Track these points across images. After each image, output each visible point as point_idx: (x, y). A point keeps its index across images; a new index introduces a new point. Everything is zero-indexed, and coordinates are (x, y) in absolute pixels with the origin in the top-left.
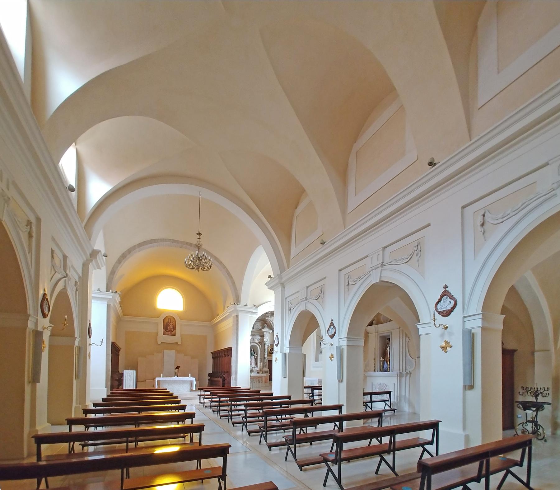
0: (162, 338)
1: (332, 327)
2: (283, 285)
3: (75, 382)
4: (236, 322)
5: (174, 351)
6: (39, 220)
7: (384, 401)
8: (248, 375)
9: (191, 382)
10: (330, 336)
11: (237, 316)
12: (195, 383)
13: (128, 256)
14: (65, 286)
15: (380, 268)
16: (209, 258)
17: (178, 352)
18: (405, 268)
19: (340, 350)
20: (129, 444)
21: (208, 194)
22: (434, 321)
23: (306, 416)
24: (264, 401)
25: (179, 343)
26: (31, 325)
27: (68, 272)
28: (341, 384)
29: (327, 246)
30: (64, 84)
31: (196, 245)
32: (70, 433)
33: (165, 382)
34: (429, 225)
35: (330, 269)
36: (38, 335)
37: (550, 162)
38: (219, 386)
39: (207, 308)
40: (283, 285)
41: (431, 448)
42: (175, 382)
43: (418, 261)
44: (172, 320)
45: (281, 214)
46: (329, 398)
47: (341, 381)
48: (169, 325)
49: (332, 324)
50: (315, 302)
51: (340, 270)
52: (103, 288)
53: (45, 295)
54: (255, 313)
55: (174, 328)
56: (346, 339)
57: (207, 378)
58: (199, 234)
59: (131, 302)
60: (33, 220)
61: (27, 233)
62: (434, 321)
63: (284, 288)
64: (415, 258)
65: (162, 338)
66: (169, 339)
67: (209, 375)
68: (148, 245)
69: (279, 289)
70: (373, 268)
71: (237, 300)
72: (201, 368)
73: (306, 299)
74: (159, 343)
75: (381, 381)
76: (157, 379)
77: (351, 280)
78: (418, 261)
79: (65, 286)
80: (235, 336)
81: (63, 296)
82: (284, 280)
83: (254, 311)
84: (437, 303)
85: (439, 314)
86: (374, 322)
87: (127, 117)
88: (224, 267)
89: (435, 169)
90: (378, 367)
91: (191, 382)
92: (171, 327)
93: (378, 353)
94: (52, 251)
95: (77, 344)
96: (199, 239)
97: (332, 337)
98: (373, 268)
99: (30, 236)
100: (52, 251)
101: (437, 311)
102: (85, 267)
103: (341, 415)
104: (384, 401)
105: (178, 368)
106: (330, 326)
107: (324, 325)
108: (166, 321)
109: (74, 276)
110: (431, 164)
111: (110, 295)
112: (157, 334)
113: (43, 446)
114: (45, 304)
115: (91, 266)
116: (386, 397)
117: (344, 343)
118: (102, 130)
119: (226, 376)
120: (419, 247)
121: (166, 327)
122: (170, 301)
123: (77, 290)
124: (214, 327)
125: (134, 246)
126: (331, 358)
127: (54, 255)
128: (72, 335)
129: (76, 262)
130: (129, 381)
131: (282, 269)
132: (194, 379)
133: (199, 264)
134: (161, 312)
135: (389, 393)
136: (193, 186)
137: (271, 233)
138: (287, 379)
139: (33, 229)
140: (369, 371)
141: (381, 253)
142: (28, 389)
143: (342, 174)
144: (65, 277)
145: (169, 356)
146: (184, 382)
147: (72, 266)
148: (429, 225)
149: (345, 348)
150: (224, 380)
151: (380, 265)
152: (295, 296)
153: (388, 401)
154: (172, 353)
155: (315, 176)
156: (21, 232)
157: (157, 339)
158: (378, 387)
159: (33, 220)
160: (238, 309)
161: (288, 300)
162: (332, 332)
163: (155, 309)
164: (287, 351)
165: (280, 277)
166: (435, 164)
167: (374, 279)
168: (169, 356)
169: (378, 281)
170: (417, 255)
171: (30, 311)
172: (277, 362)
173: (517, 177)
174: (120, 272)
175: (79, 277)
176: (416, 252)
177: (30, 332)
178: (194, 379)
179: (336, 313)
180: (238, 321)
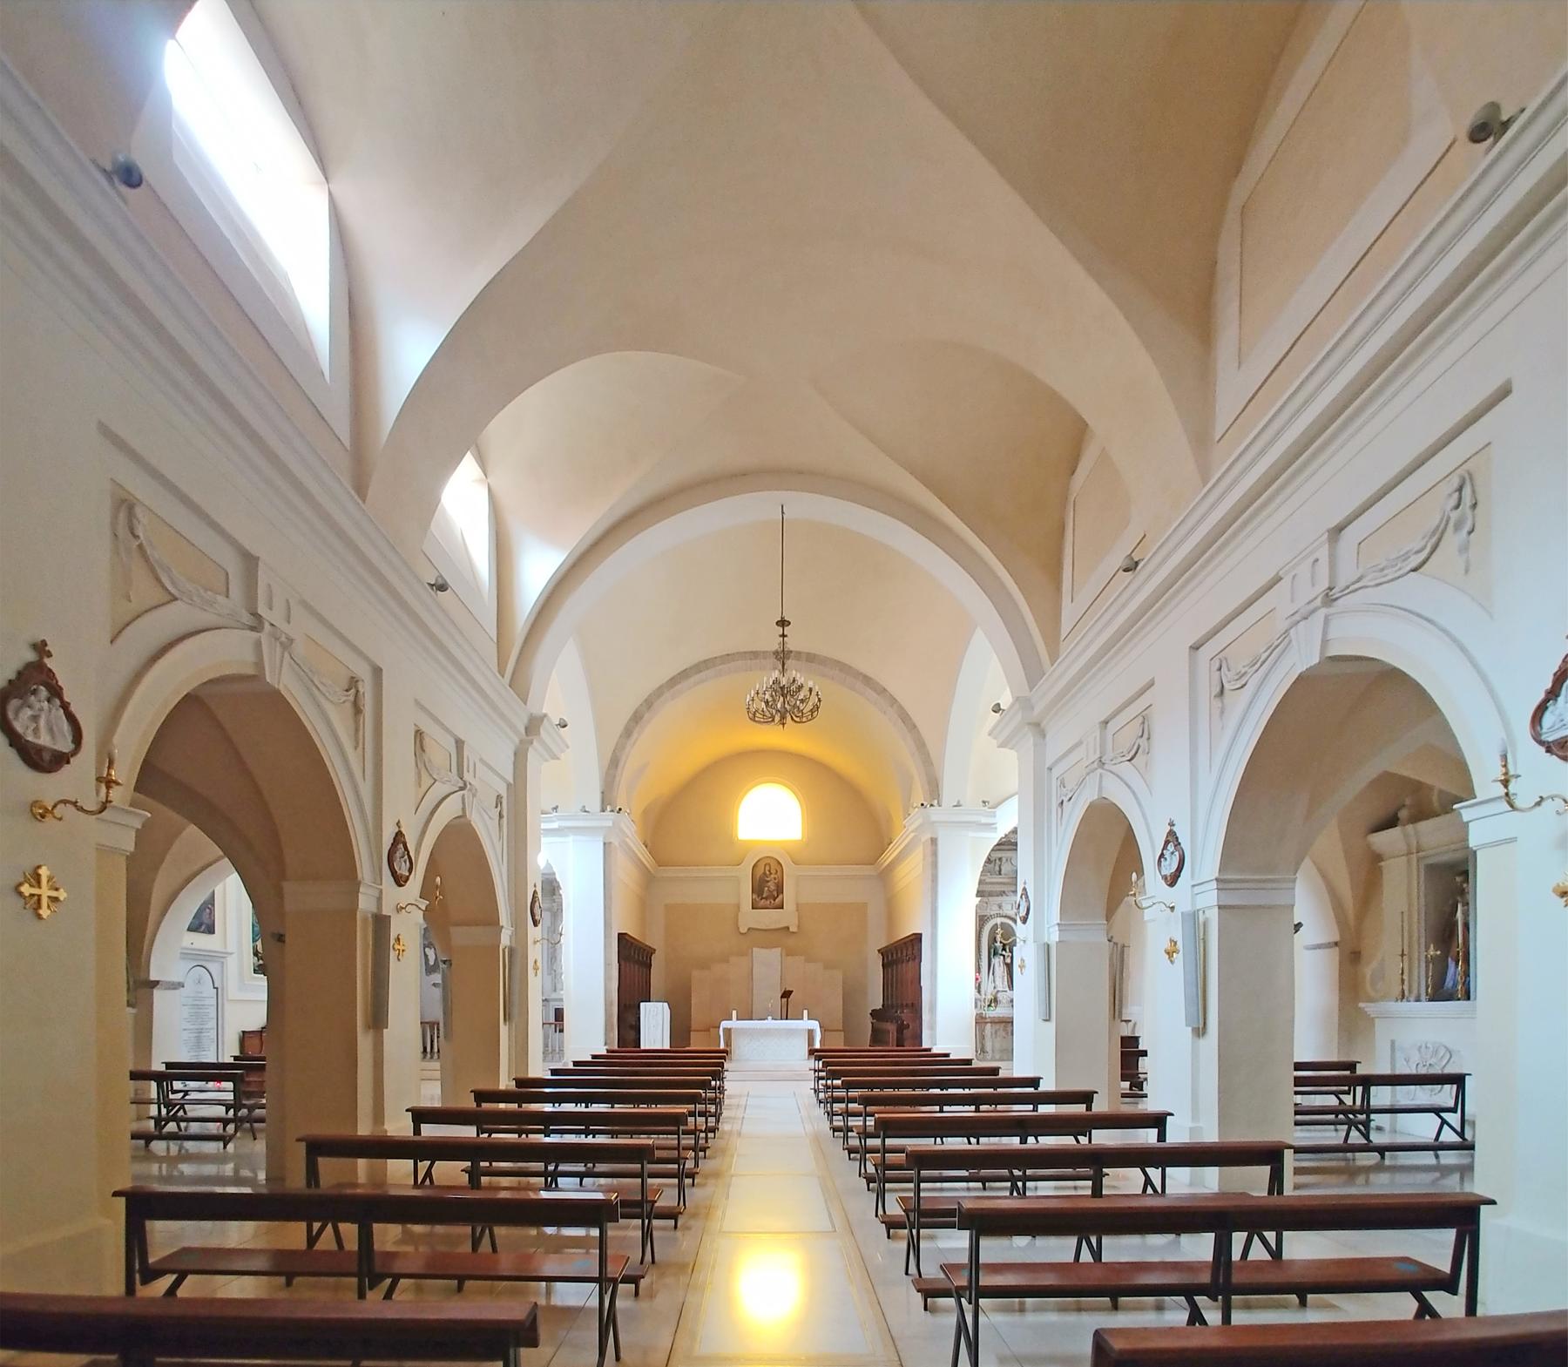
0: (752, 918)
1: (1171, 847)
2: (1038, 728)
3: (504, 1030)
4: (929, 859)
6: (377, 672)
7: (1437, 1111)
8: (971, 1013)
9: (811, 1033)
10: (1165, 878)
11: (934, 841)
13: (646, 716)
14: (464, 809)
15: (1323, 611)
16: (810, 684)
17: (790, 952)
18: (1413, 591)
19: (1193, 921)
20: (650, 1181)
21: (805, 506)
22: (1505, 783)
23: (1024, 1141)
24: (1000, 1090)
26: (365, 903)
27: (467, 777)
28: (1202, 1042)
29: (1150, 567)
30: (409, 350)
31: (776, 653)
32: (417, 1138)
34: (1504, 392)
35: (1163, 651)
36: (381, 923)
38: (887, 1044)
39: (861, 824)
40: (1038, 728)
41: (1449, 1306)
43: (1464, 549)
44: (774, 866)
45: (1023, 503)
46: (1186, 1092)
47: (1200, 1031)
49: (1172, 838)
50: (1126, 769)
51: (1195, 648)
52: (594, 803)
53: (399, 837)
54: (990, 827)
55: (780, 889)
56: (1214, 885)
57: (868, 1022)
58: (783, 623)
59: (671, 830)
60: (364, 673)
61: (349, 705)
62: (1505, 783)
63: (1044, 736)
64: (1452, 541)
65: (752, 918)
67: (874, 1013)
68: (692, 680)
69: (1029, 740)
70: (1297, 617)
71: (934, 791)
72: (851, 995)
73: (1102, 764)
75: (1411, 1032)
76: (725, 1024)
77: (1231, 675)
78: (1464, 549)
79: (464, 809)
81: (460, 836)
82: (1037, 710)
83: (984, 820)
84: (1541, 710)
85: (1549, 750)
86: (1403, 814)
87: (571, 367)
88: (893, 701)
89: (1507, 147)
90: (1421, 978)
93: (1419, 928)
94: (419, 734)
95: (505, 939)
96: (783, 636)
97: (1173, 880)
98: (1297, 617)
99: (357, 710)
100: (419, 734)
101: (1541, 743)
102: (520, 758)
103: (1161, 1145)
104: (1437, 1111)
106: (1167, 843)
107: (1149, 846)
108: (760, 871)
109: (490, 781)
110: (1485, 129)
111: (608, 819)
112: (738, 907)
113: (323, 1163)
114: (398, 855)
115: (531, 755)
116: (1446, 1095)
117: (1209, 899)
118: (529, 418)
119: (906, 1015)
120: (1467, 491)
121: (759, 887)
122: (770, 816)
123: (501, 816)
124: (885, 877)
126: (1170, 954)
127: (427, 741)
128: (493, 922)
129: (492, 752)
130: (655, 1026)
131: (1033, 673)
132: (815, 1025)
133: (785, 704)
134: (749, 846)
135: (1458, 1080)
136: (765, 494)
137: (997, 578)
138: (1052, 1026)
139: (362, 698)
140: (1384, 998)
141: (1323, 553)
142: (364, 1043)
143: (1185, 300)
144: (462, 789)
145: (768, 966)
146: (791, 1032)
147: (481, 760)
148: (1504, 392)
149: (1213, 916)
150: (901, 1029)
151: (1318, 602)
152: (1074, 758)
153: (1454, 1110)
154: (775, 954)
155: (1095, 351)
156: (328, 706)
158: (1416, 1058)
159: (364, 673)
160: (934, 818)
161: (1056, 772)
162: (1170, 866)
163: (730, 839)
164: (1054, 936)
165: (1022, 702)
166: (1506, 125)
167: (1303, 657)
168: (768, 966)
169: (1317, 661)
170: (1458, 527)
171: (364, 870)
172: (1025, 971)
174: (633, 759)
175: (509, 785)
176: (1454, 515)
177: (365, 920)
178: (815, 1025)
179: (1186, 795)
180: (935, 854)
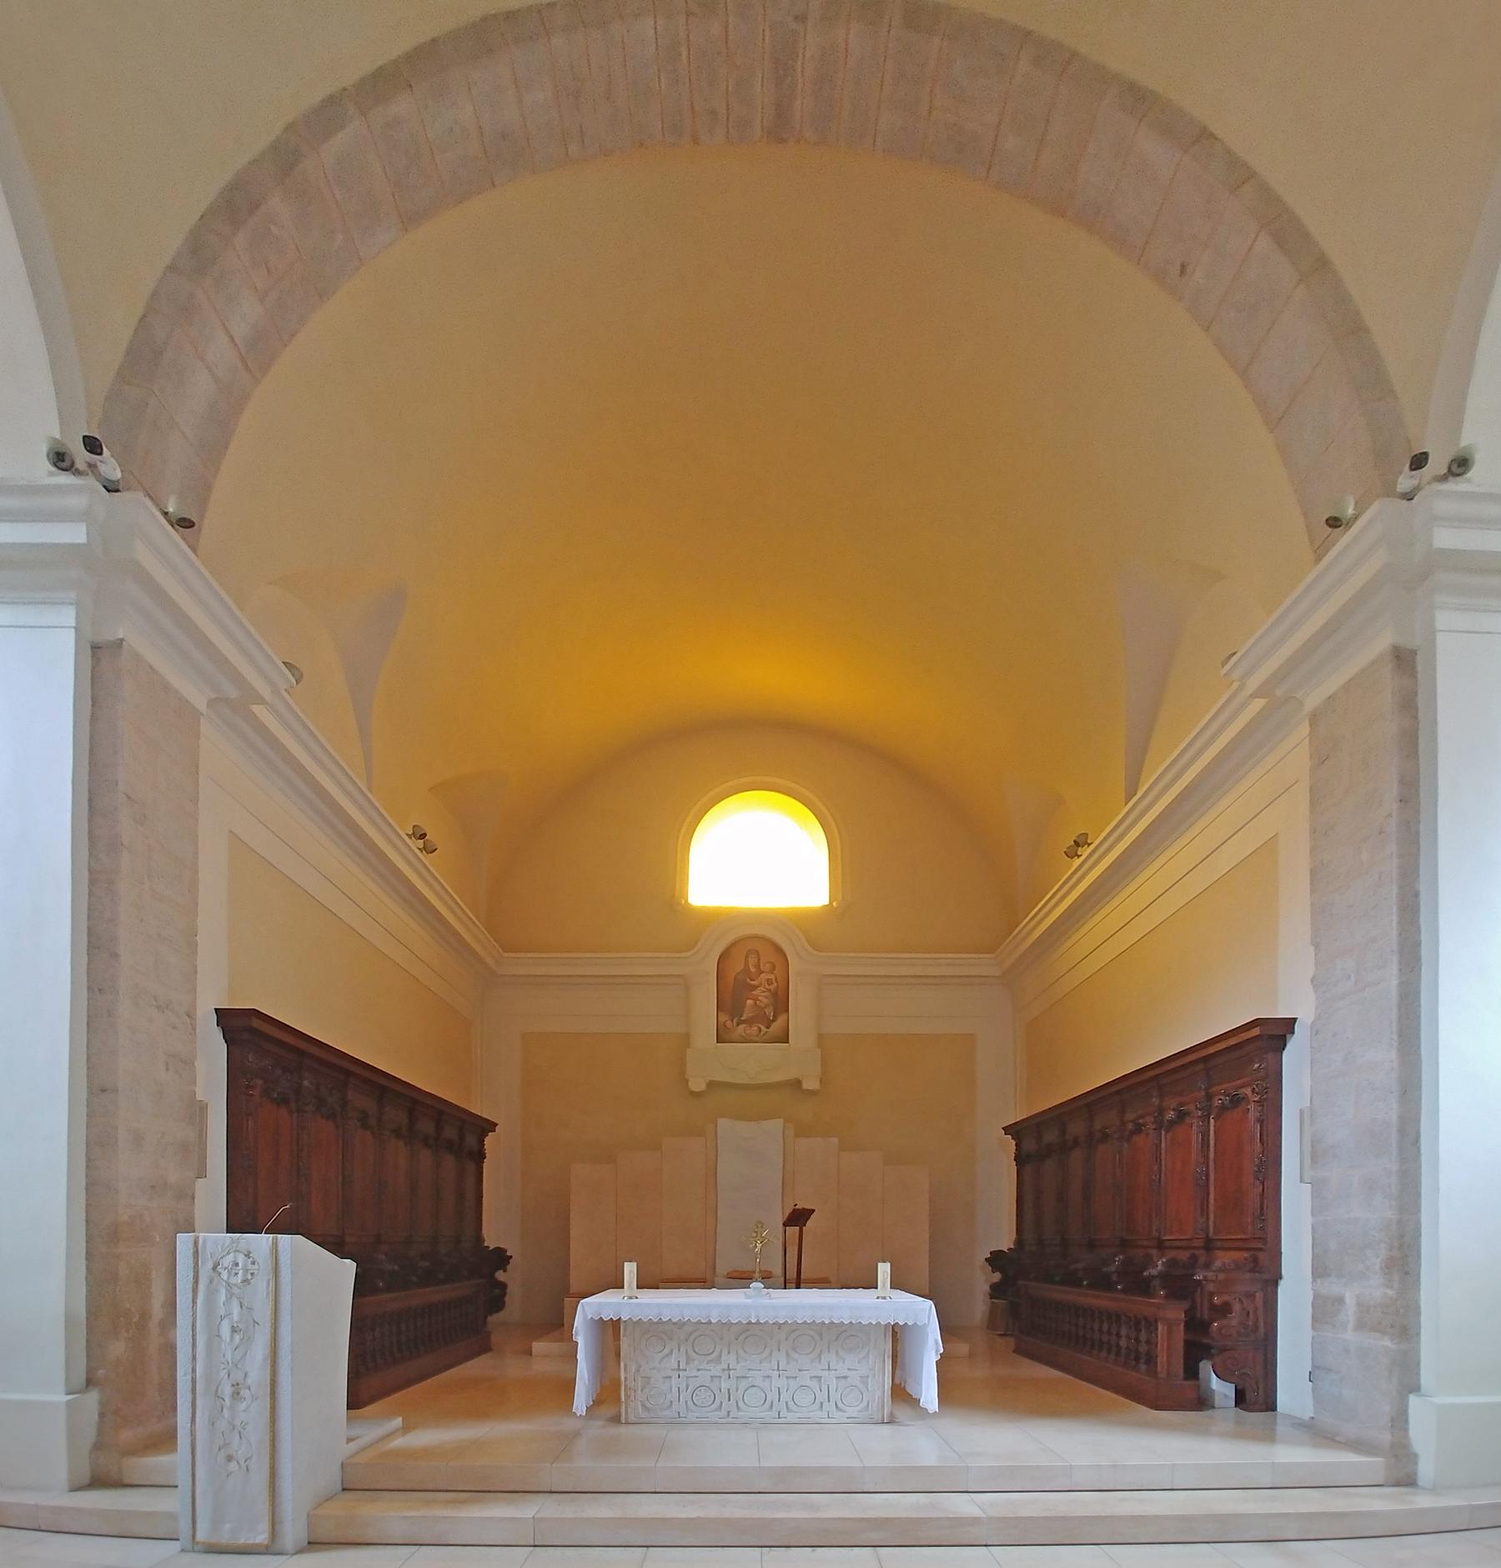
0: (716, 1060)
5: (775, 1126)
12: (930, 1348)
25: (810, 1084)
33: (660, 1331)
37: (793, 1231)
42: (750, 1334)
48: (753, 972)
55: (781, 1002)
66: (753, 1061)
67: (996, 1260)
74: (697, 1085)
80: (1391, 919)
91: (897, 1335)
92: (764, 998)
105: (798, 1218)
112: (686, 1039)
121: (731, 1001)
125: (332, 101)
157: (682, 1062)
173: (265, 1495)
